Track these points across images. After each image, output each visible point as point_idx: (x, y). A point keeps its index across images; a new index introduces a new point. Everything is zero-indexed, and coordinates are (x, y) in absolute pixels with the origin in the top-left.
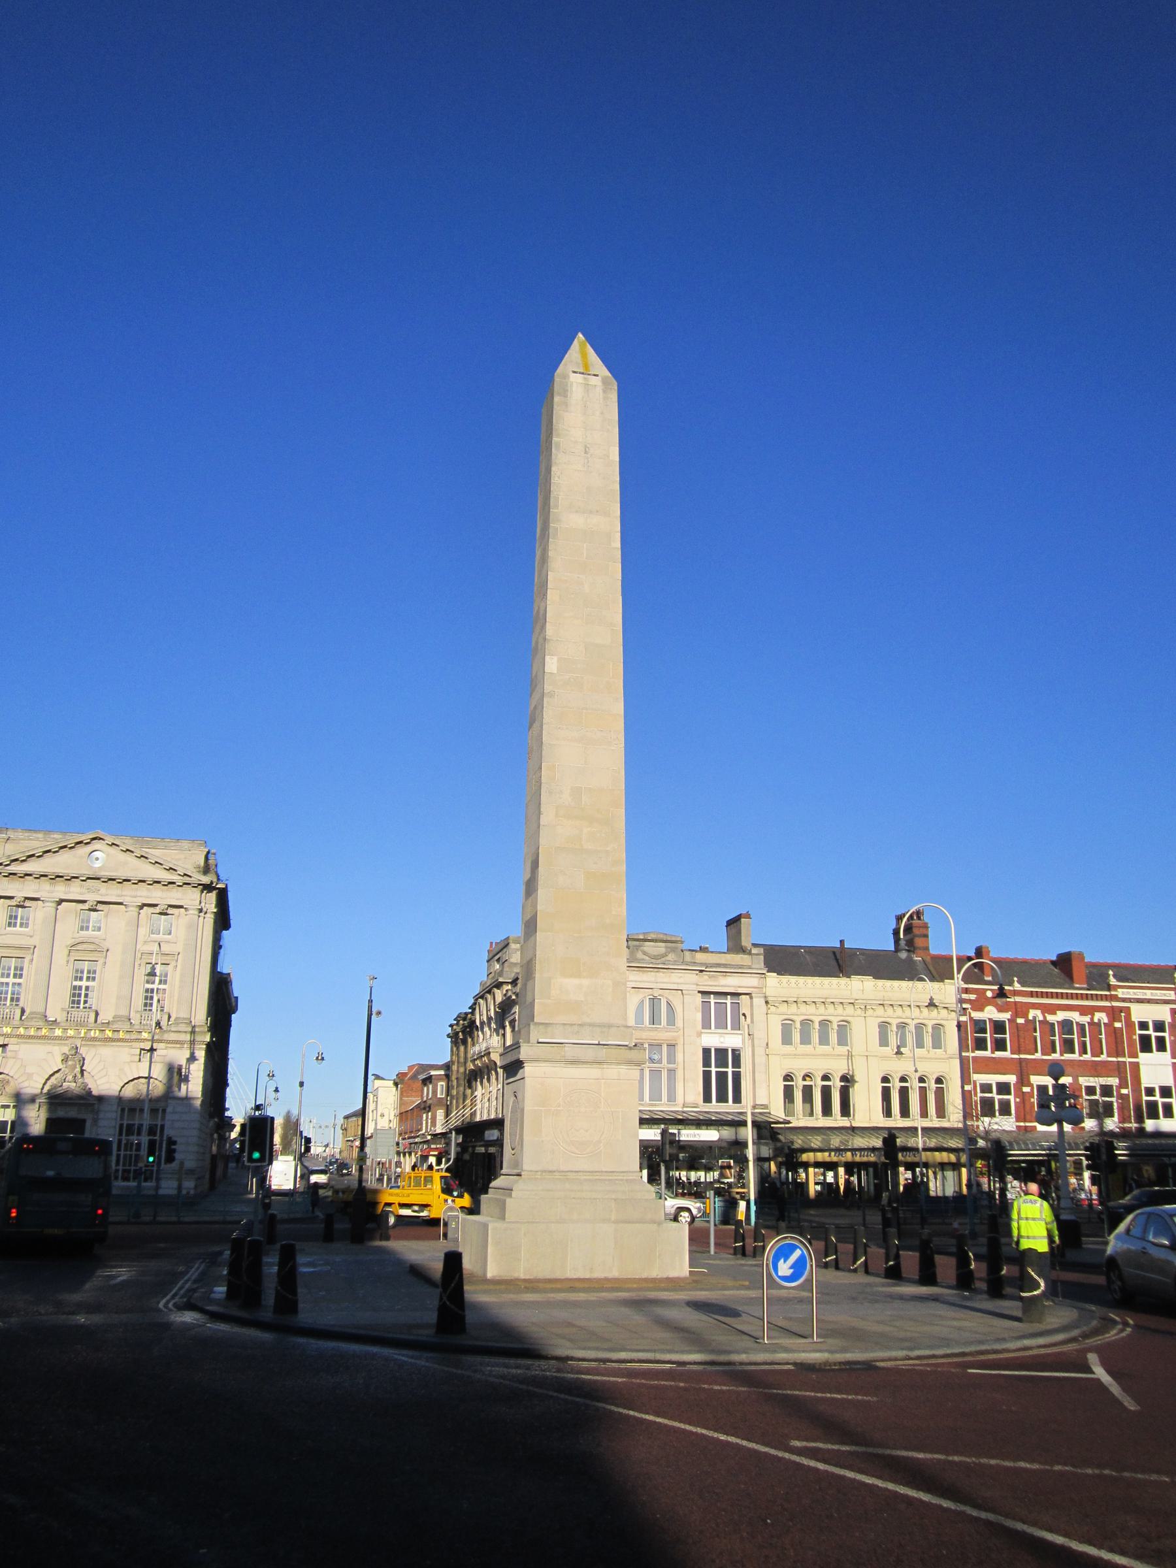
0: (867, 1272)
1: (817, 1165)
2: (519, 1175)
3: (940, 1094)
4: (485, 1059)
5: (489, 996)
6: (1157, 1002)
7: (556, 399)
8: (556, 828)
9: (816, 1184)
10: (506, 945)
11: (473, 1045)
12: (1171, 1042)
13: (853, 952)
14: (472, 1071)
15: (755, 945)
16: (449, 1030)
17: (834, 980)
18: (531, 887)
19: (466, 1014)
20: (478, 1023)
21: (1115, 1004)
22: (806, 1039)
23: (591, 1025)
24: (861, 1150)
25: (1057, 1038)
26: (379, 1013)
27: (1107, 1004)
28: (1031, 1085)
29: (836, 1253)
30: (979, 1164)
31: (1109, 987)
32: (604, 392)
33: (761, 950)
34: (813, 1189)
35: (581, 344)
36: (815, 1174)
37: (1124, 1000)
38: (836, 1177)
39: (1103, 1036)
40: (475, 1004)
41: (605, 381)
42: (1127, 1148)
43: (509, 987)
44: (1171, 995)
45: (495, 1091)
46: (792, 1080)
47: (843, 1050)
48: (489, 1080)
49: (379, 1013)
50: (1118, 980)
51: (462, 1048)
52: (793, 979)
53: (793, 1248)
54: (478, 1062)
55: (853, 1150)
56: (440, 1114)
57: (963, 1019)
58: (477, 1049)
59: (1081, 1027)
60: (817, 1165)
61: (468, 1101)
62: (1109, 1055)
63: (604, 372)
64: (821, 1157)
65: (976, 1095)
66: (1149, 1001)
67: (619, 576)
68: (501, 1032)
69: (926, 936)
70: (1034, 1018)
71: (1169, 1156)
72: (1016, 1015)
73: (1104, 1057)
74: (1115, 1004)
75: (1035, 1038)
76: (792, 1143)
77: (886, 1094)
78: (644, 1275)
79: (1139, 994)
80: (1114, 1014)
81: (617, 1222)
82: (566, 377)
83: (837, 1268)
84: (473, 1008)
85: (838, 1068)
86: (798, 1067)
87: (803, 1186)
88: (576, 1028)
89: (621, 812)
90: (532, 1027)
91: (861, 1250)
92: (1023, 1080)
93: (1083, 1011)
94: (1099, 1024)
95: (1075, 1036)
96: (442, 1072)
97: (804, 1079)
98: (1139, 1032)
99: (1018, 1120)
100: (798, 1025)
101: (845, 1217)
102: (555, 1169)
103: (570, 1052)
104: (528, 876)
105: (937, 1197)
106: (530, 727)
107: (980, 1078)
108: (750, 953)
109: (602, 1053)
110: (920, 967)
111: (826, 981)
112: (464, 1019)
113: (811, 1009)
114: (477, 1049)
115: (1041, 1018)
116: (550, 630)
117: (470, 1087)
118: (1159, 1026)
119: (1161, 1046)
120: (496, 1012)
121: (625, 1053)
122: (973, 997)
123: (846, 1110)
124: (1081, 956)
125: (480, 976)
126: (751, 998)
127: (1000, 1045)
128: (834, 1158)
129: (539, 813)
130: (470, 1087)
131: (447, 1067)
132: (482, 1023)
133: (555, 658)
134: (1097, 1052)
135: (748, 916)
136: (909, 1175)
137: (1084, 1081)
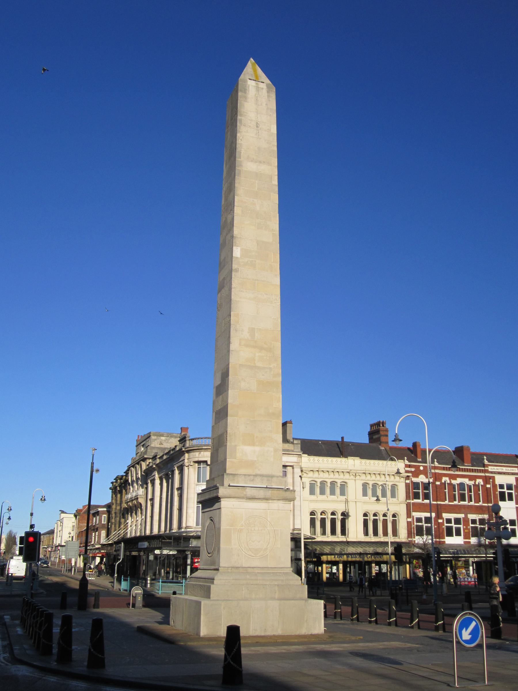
0: (419, 628)
1: (328, 562)
2: (217, 570)
4: (135, 502)
5: (138, 467)
6: (508, 474)
7: (240, 94)
8: (240, 353)
9: (327, 573)
10: (148, 437)
11: (126, 494)
12: (515, 495)
13: (348, 444)
14: (125, 509)
15: (294, 439)
16: (111, 485)
17: (339, 459)
18: (222, 389)
19: (122, 476)
20: (130, 481)
21: (487, 474)
22: (322, 492)
23: (262, 476)
24: (351, 554)
25: (457, 493)
26: (97, 471)
27: (483, 474)
28: (443, 519)
29: (396, 617)
30: (415, 562)
31: (484, 465)
32: (268, 92)
33: (299, 442)
34: (325, 576)
35: (253, 65)
36: (327, 568)
37: (492, 472)
38: (338, 569)
39: (481, 492)
40: (128, 470)
41: (268, 86)
42: (494, 553)
43: (150, 461)
44: (515, 470)
45: (140, 521)
46: (315, 515)
47: (343, 498)
48: (136, 514)
49: (97, 471)
50: (489, 462)
51: (119, 496)
52: (316, 458)
53: (470, 621)
54: (130, 504)
55: (348, 555)
56: (103, 533)
57: (408, 481)
58: (129, 496)
59: (469, 487)
60: (328, 562)
61: (122, 526)
62: (483, 503)
63: (268, 81)
64: (331, 558)
65: (414, 524)
66: (504, 473)
67: (277, 202)
68: (145, 486)
69: (387, 436)
70: (445, 481)
71: (516, 557)
72: (436, 480)
73: (481, 503)
74: (487, 474)
75: (445, 492)
76: (316, 550)
77: (366, 523)
78: (298, 633)
79: (500, 469)
80: (487, 480)
81: (280, 599)
82: (245, 81)
83: (396, 625)
84: (127, 473)
85: (340, 508)
86: (319, 507)
87: (320, 574)
88: (252, 477)
89: (278, 345)
90: (225, 476)
91: (415, 615)
92: (439, 516)
93: (471, 478)
94: (478, 485)
95: (466, 492)
96: (105, 509)
97: (321, 514)
98: (499, 490)
99: (464, 538)
100: (319, 484)
101: (345, 592)
102: (239, 566)
103: (249, 492)
104: (218, 382)
105: (396, 581)
106: (219, 291)
107: (416, 515)
108: (293, 443)
109: (269, 493)
110: (384, 453)
111: (334, 459)
112: (121, 479)
113: (326, 475)
114: (129, 496)
115: (449, 482)
116: (236, 231)
117: (124, 517)
118: (509, 487)
119: (510, 498)
120: (141, 475)
121: (282, 493)
122: (413, 470)
123: (344, 532)
124: (468, 448)
125: (130, 454)
126: (293, 468)
128: (337, 559)
129: (229, 343)
130: (124, 517)
131: (109, 506)
132: (133, 481)
133: (239, 248)
134: (477, 500)
135: (291, 422)
136: (377, 568)
137: (471, 517)
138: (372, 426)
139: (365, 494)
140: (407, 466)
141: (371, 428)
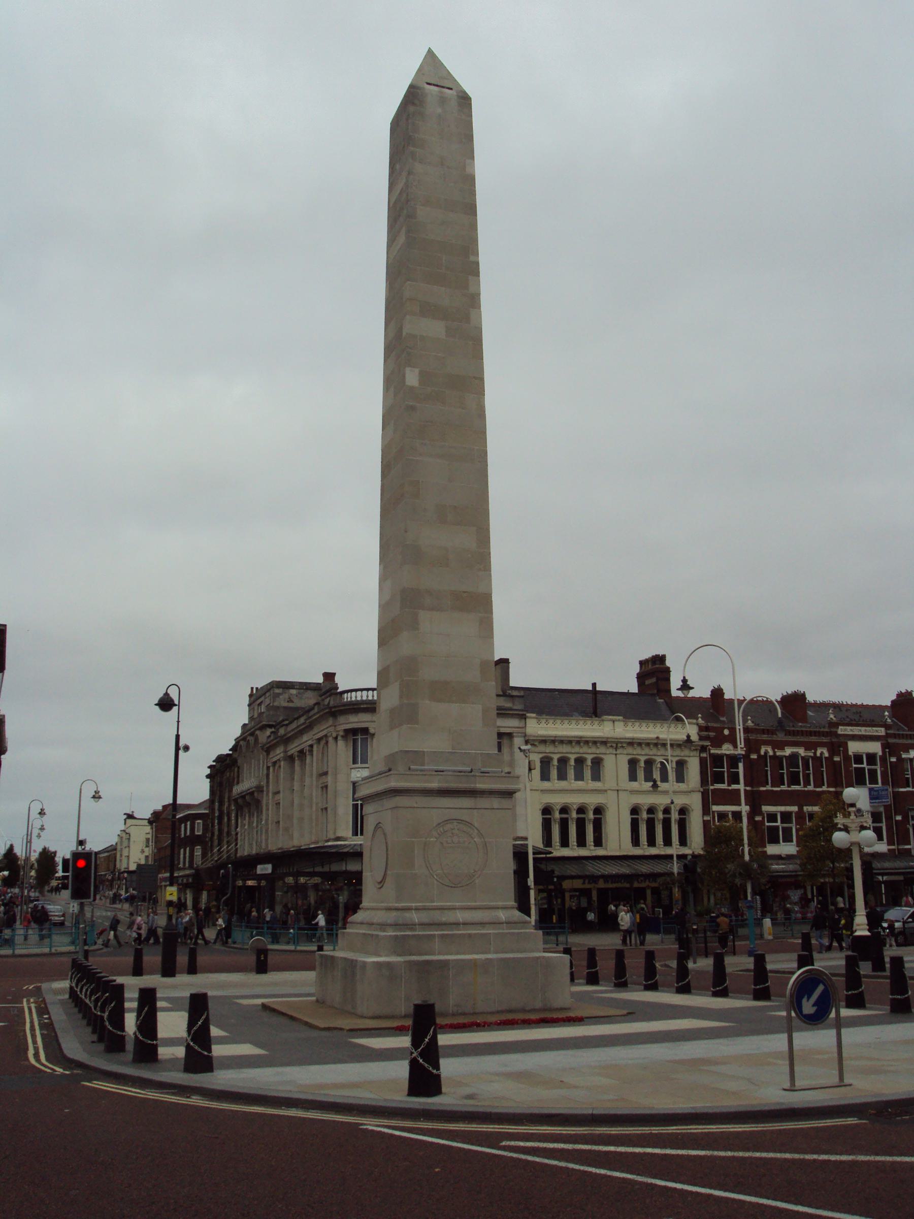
3: (682, 824)
56: (198, 851)
57: (704, 755)
73: (824, 788)
77: (635, 825)
86: (558, 800)
115: (771, 753)
123: (598, 842)
127: (794, 780)
134: (807, 783)
138: (641, 663)
139: (633, 777)
140: (701, 729)
141: (641, 667)
